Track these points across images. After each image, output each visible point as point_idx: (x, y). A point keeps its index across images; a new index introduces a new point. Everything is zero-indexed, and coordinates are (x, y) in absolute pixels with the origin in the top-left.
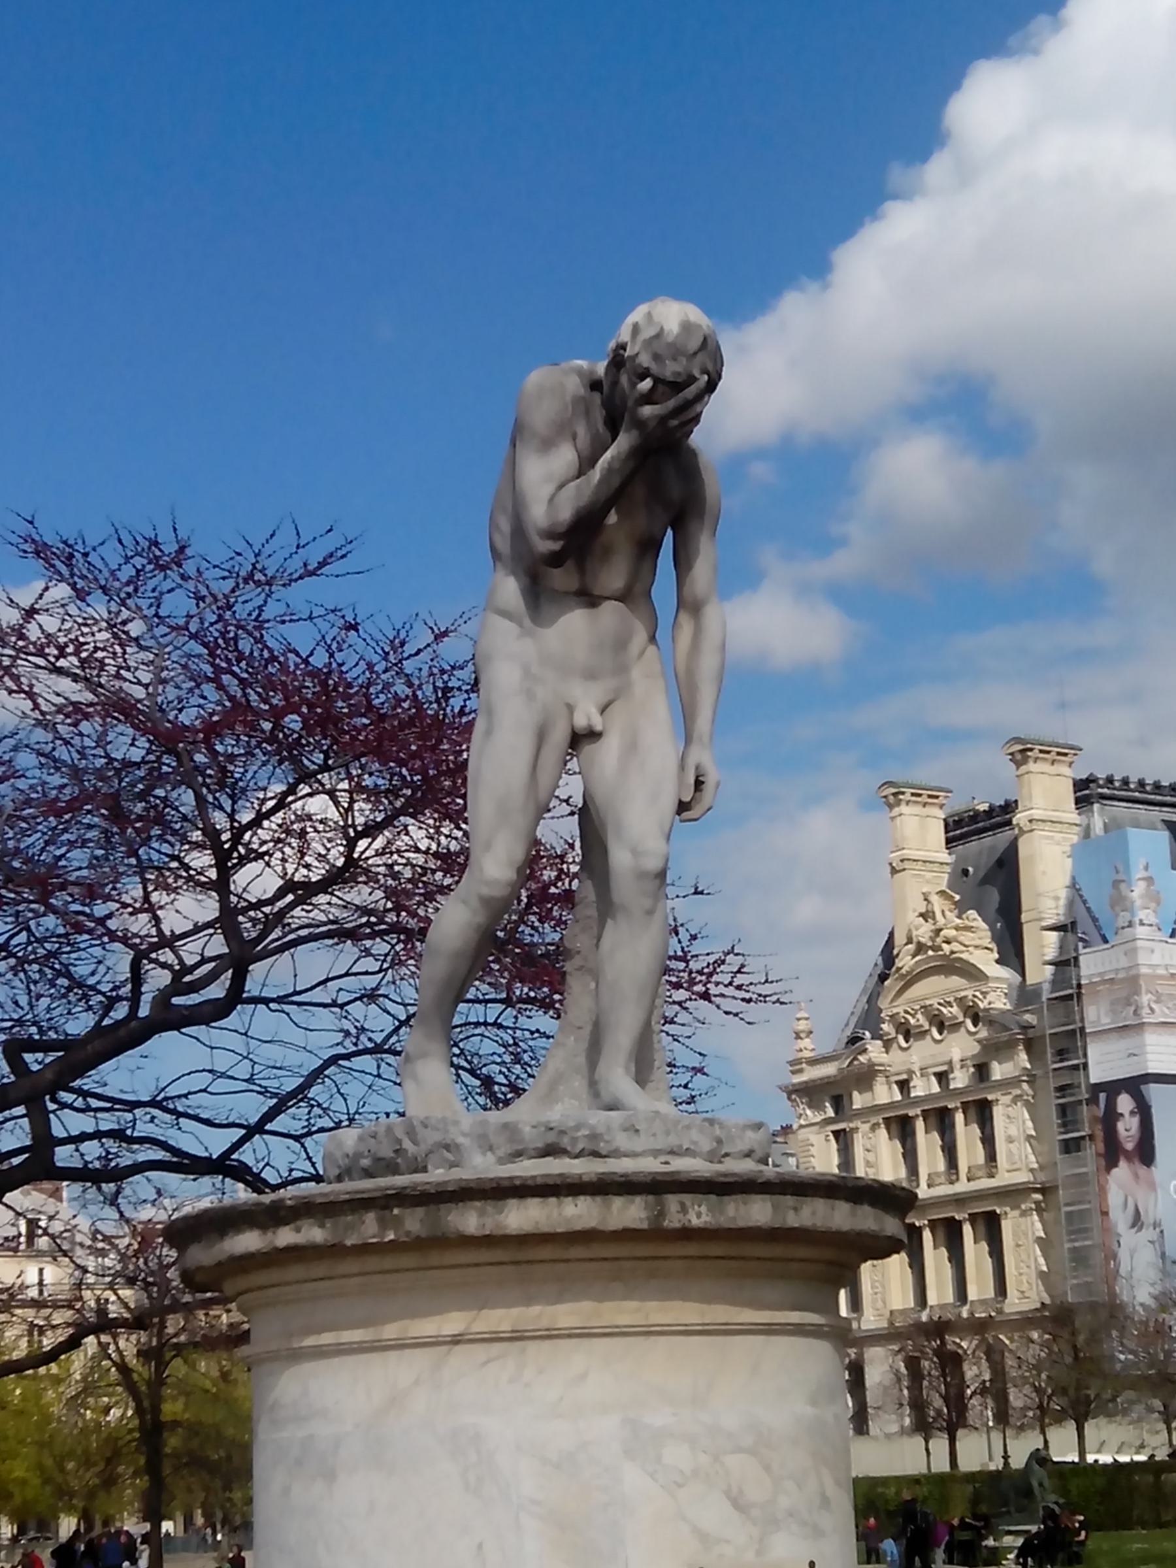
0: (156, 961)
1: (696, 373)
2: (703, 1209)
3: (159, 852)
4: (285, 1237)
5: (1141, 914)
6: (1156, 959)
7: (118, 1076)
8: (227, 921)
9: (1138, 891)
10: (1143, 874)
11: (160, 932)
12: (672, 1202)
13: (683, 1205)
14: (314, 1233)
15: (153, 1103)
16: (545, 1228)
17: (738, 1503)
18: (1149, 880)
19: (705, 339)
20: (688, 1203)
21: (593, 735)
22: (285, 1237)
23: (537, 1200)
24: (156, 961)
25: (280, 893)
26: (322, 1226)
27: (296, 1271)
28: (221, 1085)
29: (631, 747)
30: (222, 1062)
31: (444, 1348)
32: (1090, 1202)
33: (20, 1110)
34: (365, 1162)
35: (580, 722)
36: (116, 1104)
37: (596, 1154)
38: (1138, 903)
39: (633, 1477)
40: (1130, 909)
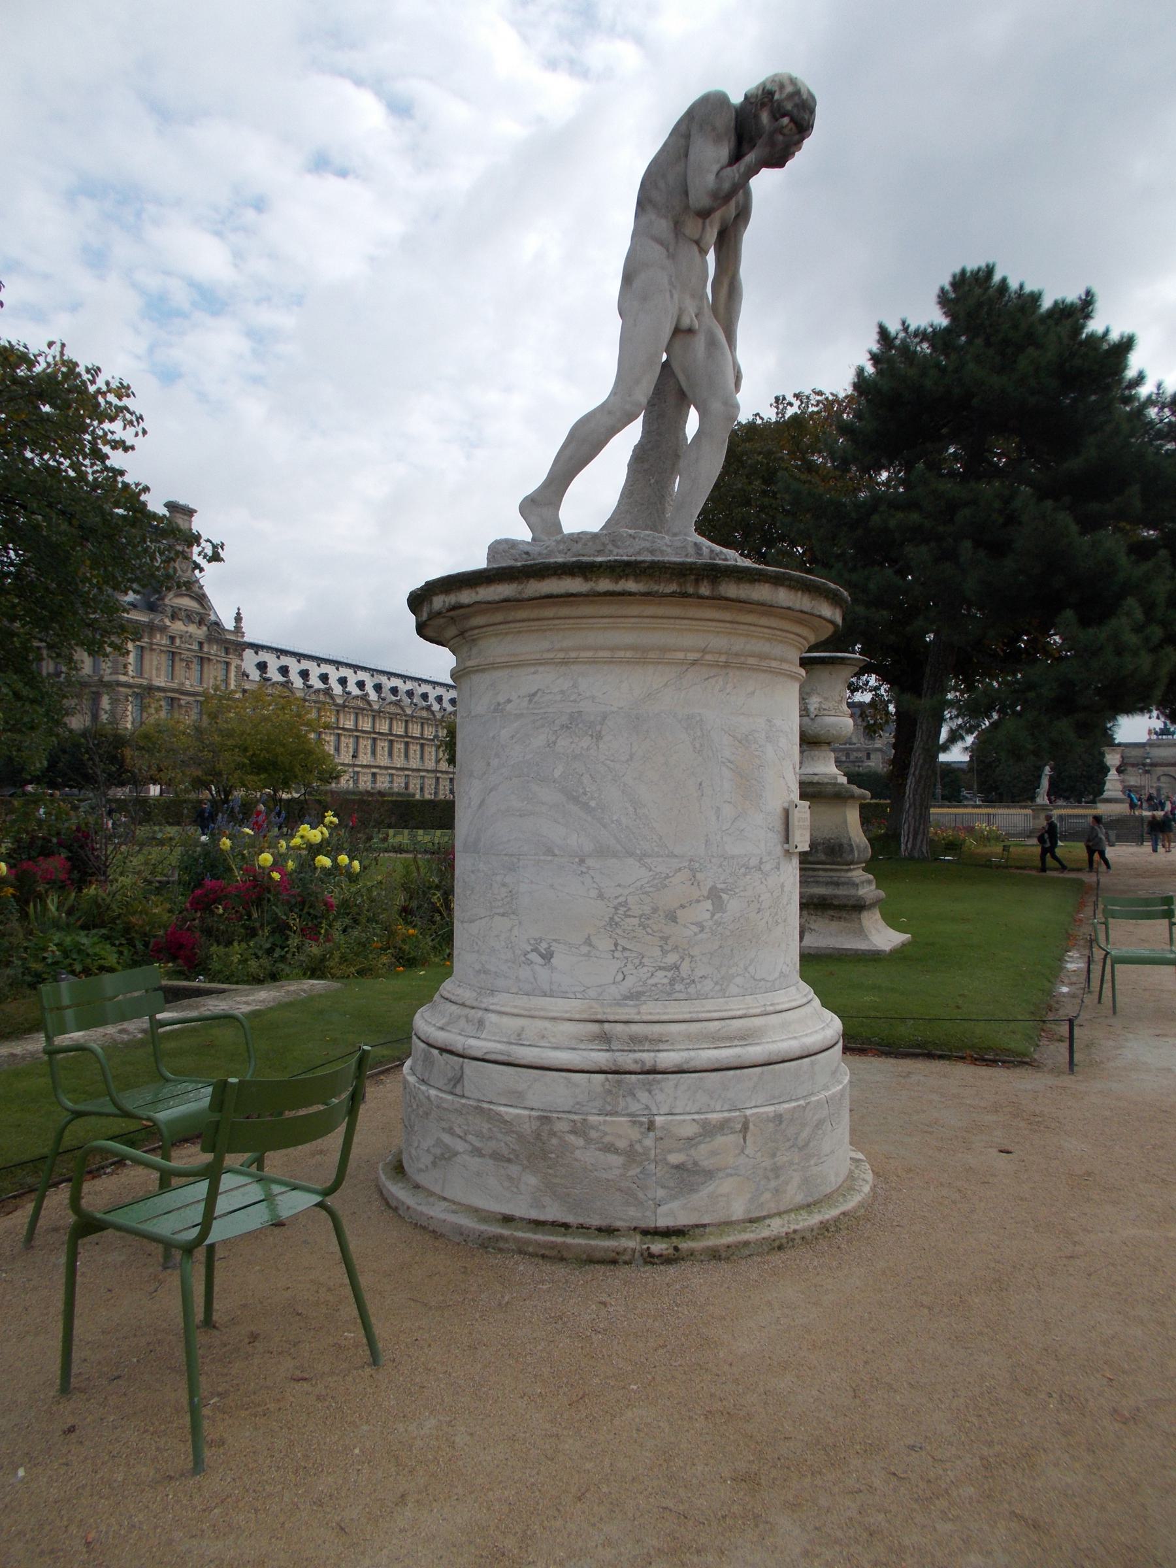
35: (686, 322)
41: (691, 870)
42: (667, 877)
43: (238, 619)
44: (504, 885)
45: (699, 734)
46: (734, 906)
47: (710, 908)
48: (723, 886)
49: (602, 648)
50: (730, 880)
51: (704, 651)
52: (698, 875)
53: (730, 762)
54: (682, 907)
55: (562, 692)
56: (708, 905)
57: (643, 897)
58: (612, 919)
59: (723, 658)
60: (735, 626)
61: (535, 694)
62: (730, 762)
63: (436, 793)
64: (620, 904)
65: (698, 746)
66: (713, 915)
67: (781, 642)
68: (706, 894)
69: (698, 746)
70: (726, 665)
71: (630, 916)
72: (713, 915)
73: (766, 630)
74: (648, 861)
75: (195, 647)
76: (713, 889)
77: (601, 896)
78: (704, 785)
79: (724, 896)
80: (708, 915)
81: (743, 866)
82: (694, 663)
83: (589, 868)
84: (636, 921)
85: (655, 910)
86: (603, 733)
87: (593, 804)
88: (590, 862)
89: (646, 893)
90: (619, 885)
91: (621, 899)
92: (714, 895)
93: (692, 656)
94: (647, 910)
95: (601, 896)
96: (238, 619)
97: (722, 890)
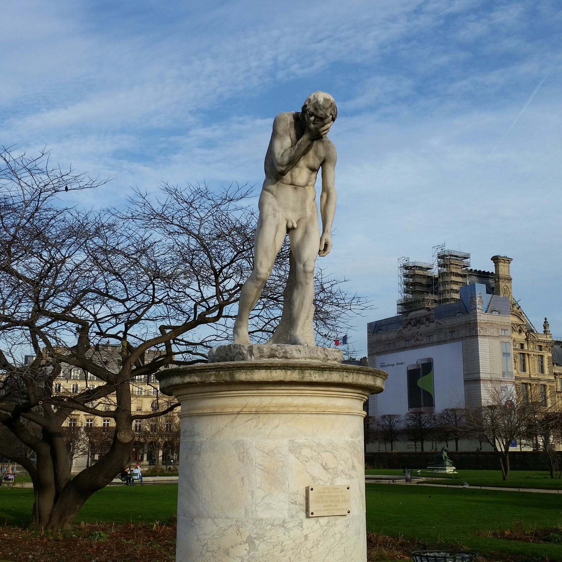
0: (202, 305)
1: (328, 114)
2: (317, 376)
3: (9, 213)
4: (187, 379)
5: (478, 306)
6: (481, 318)
7: (190, 336)
8: (219, 293)
9: (478, 300)
10: (479, 295)
11: (202, 297)
12: (307, 373)
13: (310, 374)
14: (196, 379)
15: (201, 344)
16: (265, 380)
17: (325, 468)
18: (481, 297)
19: (331, 104)
20: (312, 374)
21: (293, 228)
22: (187, 379)
23: (264, 371)
24: (202, 305)
25: (235, 287)
26: (198, 376)
27: (191, 390)
28: (218, 339)
29: (306, 232)
30: (219, 333)
31: (235, 416)
32: (385, 377)
33: (164, 344)
34: (217, 358)
35: (290, 225)
36: (188, 344)
37: (287, 358)
38: (477, 303)
39: (292, 458)
40: (475, 305)
41: (237, 526)
42: (225, 530)
43: (546, 325)
46: (262, 547)
48: (255, 536)
49: (520, 461)
50: (260, 533)
52: (241, 530)
53: (260, 465)
54: (232, 547)
62: (260, 465)
63: (129, 334)
65: (241, 457)
66: (249, 552)
68: (245, 540)
72: (249, 552)
75: (518, 346)
76: (249, 537)
78: (244, 479)
80: (245, 553)
81: (270, 524)
85: (219, 548)
96: (546, 325)
97: (255, 538)
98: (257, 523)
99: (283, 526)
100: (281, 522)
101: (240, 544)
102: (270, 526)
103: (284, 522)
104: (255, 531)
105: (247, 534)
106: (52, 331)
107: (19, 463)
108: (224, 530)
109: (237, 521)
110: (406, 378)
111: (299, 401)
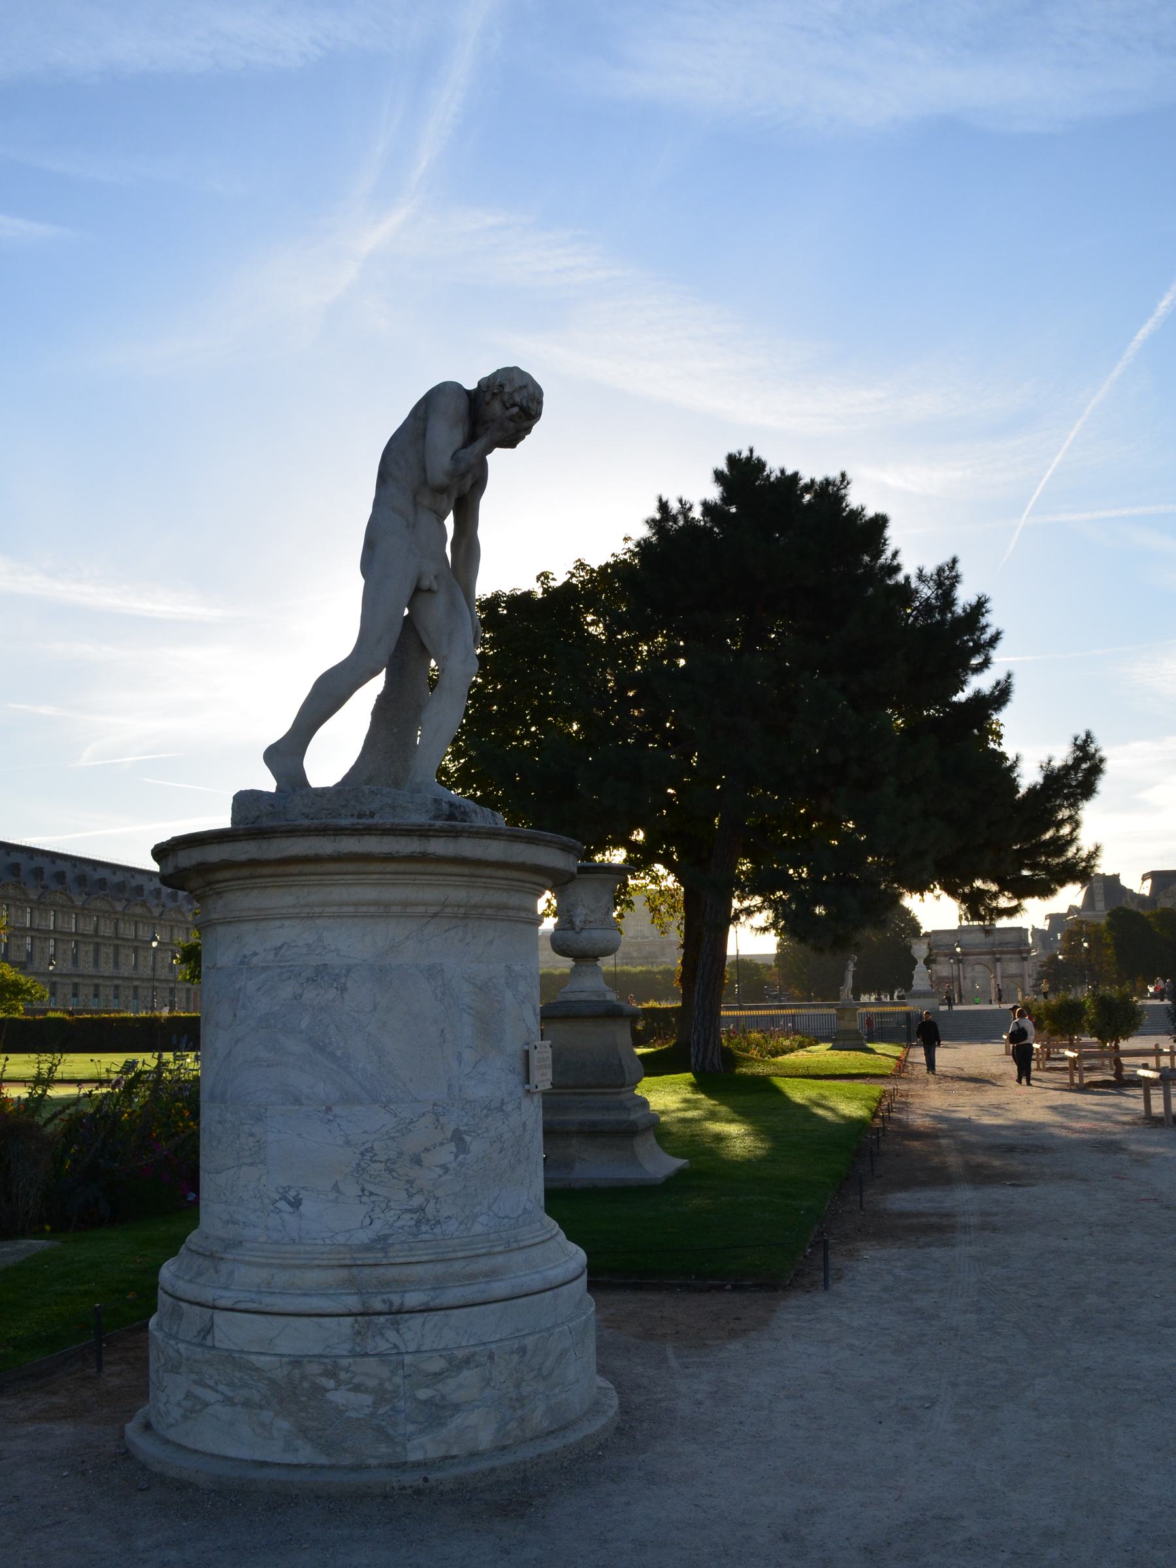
35: (425, 584)
41: (435, 1114)
42: (412, 1122)
44: (252, 1135)
45: (440, 983)
47: (454, 1150)
48: (465, 1128)
51: (444, 905)
54: (427, 1150)
55: (308, 945)
56: (452, 1147)
57: (388, 1142)
58: (358, 1165)
59: (462, 910)
60: (474, 879)
61: (281, 947)
64: (366, 1150)
66: (456, 1156)
67: (518, 891)
69: (439, 995)
70: (466, 917)
71: (376, 1161)
72: (456, 1156)
73: (503, 882)
74: (393, 1107)
77: (348, 1143)
79: (467, 1138)
80: (452, 1157)
82: (434, 916)
83: (335, 1116)
84: (382, 1166)
85: (400, 1154)
86: (348, 985)
87: (339, 1053)
88: (337, 1110)
89: (393, 1138)
90: (365, 1132)
91: (367, 1146)
92: (458, 1137)
93: (433, 910)
94: (393, 1154)
95: (348, 1143)
97: (465, 1132)
98: (468, 1106)
99: (502, 1110)
100: (499, 1104)
101: (442, 1144)
102: (485, 1111)
103: (503, 1103)
104: (465, 1121)
105: (452, 1126)
106: (467, 1374)
107: (825, 1040)
108: (410, 1123)
109: (435, 1105)
110: (28, 845)
111: (339, 894)
